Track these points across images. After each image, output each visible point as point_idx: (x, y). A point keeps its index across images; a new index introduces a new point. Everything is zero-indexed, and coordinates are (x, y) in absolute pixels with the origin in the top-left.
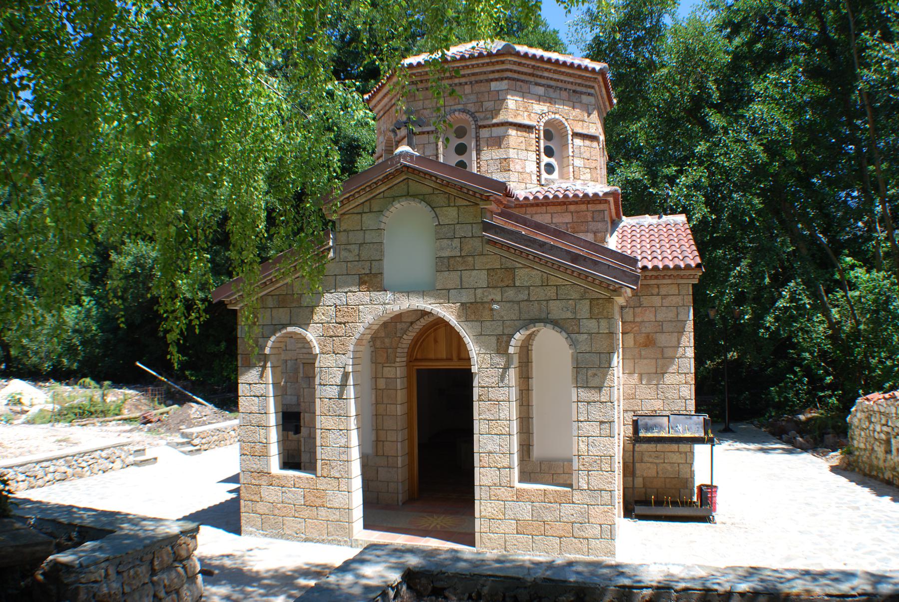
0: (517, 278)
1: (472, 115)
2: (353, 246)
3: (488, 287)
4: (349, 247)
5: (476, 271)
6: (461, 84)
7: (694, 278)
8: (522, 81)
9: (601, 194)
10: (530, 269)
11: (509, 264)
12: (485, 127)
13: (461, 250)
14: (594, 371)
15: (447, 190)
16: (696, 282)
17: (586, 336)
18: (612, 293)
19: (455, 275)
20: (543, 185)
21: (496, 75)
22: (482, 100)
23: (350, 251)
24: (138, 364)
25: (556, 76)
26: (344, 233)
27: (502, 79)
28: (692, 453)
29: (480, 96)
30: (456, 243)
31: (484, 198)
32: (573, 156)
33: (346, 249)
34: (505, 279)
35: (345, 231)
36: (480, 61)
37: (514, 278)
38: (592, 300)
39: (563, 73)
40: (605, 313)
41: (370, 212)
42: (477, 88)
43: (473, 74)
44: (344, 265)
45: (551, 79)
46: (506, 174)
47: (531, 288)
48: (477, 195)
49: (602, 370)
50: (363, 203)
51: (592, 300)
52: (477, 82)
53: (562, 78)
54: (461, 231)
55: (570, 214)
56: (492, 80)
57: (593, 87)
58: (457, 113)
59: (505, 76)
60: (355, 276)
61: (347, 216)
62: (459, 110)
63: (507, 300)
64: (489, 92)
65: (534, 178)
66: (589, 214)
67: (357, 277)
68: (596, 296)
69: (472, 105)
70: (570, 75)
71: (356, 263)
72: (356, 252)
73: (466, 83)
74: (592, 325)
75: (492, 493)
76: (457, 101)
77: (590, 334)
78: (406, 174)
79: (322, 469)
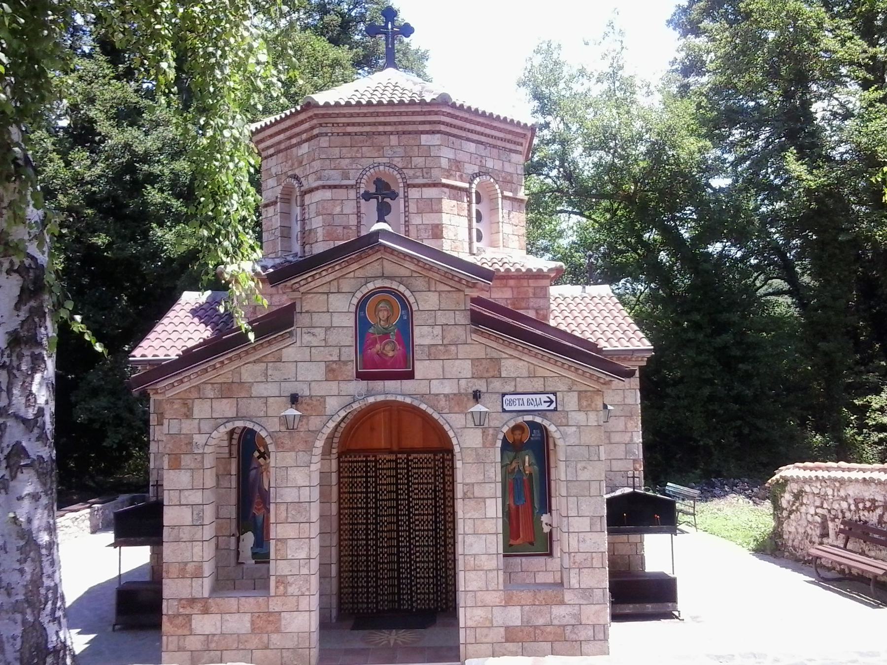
0: (503, 369)
1: (400, 171)
2: (318, 329)
4: (313, 330)
5: (460, 361)
6: (385, 133)
7: (642, 360)
8: (454, 136)
9: (545, 270)
11: (495, 355)
12: (414, 186)
13: (443, 338)
14: (583, 464)
15: (430, 274)
16: (644, 364)
17: (574, 429)
18: (602, 386)
19: (437, 364)
20: (474, 254)
21: (427, 127)
22: (411, 154)
24: (527, 458)
25: (488, 131)
26: (306, 314)
27: (434, 132)
28: (642, 542)
29: (408, 149)
30: (438, 330)
31: (470, 285)
32: (503, 222)
34: (490, 370)
35: (307, 312)
37: (500, 369)
38: (580, 392)
39: (495, 128)
40: (593, 405)
41: (338, 292)
42: (405, 139)
43: (400, 123)
45: (482, 134)
46: (438, 242)
47: (518, 379)
50: (330, 282)
51: (580, 392)
52: (404, 133)
53: (494, 133)
54: (442, 319)
55: (510, 289)
56: (422, 132)
57: (522, 145)
58: (382, 168)
59: (438, 129)
63: (494, 391)
65: (466, 246)
66: (531, 290)
68: (584, 388)
69: (399, 159)
71: (322, 349)
73: (392, 133)
74: (580, 417)
75: (478, 599)
76: (381, 152)
77: (579, 427)
78: (382, 254)
79: (277, 587)
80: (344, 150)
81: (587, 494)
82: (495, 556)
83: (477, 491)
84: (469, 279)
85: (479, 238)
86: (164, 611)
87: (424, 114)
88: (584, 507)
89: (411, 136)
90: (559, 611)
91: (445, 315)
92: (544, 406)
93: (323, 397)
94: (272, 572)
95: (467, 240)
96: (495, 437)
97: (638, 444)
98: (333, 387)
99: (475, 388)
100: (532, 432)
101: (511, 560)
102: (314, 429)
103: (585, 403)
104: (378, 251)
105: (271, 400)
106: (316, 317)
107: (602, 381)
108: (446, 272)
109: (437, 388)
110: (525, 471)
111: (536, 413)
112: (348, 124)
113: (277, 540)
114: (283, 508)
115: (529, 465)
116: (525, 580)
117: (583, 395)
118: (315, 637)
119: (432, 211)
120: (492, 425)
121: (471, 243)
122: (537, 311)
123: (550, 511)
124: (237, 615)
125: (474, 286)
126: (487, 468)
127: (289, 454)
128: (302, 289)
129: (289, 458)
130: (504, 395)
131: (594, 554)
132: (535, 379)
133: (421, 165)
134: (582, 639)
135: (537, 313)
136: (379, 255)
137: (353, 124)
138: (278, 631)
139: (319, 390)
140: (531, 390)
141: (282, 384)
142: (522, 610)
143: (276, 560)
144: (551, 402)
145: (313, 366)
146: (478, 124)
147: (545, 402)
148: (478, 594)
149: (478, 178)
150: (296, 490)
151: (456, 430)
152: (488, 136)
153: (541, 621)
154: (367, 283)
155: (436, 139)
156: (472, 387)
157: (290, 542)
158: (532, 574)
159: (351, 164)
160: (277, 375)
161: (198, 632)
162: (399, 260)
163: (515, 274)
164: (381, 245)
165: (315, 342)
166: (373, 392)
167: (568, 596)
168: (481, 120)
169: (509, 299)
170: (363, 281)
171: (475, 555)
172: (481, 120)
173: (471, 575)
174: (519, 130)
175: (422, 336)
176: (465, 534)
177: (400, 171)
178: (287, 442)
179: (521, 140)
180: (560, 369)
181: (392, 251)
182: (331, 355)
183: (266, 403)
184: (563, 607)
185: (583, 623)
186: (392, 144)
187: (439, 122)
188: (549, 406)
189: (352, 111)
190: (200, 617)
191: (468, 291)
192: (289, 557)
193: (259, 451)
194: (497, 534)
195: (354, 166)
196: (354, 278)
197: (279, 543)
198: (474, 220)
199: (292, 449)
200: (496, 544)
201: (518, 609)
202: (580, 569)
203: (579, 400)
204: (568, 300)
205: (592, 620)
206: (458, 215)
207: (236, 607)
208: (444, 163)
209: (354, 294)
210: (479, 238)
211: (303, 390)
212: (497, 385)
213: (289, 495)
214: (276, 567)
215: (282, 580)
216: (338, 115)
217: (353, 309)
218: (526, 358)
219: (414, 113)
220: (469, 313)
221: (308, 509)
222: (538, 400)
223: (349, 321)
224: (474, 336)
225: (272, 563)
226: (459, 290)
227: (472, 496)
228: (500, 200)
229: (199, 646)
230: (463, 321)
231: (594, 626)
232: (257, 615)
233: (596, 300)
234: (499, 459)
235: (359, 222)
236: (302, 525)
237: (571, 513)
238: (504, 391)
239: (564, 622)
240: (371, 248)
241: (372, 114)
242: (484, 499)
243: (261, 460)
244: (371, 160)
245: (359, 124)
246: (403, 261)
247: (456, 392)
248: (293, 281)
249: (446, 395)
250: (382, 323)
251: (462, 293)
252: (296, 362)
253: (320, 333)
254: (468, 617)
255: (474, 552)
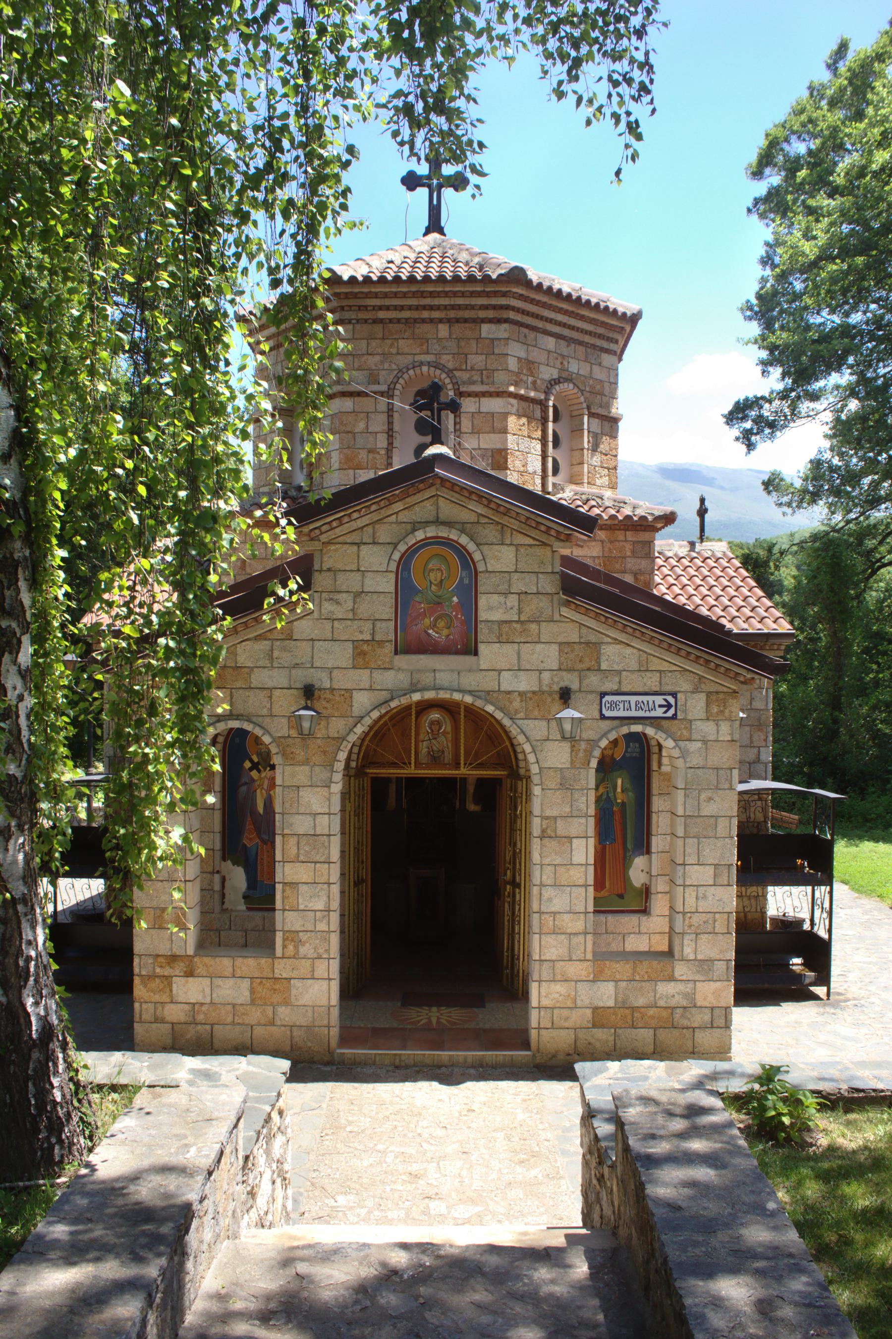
0: (603, 658)
1: (450, 372)
2: (344, 595)
3: (560, 669)
4: (337, 596)
5: (542, 646)
6: (431, 321)
8: (527, 326)
10: (622, 646)
11: (593, 638)
12: (470, 395)
13: (520, 612)
14: (709, 793)
15: (505, 520)
19: (509, 650)
21: (491, 314)
23: (338, 603)
24: (619, 781)
25: (573, 322)
27: (499, 321)
28: (764, 896)
29: (463, 344)
30: (513, 600)
31: (562, 537)
33: (331, 599)
34: (586, 659)
35: (329, 570)
36: (470, 288)
37: (598, 658)
38: (709, 694)
39: (582, 318)
41: (374, 543)
42: (458, 329)
43: (453, 307)
44: (328, 625)
47: (624, 673)
48: (553, 533)
49: (720, 792)
50: (362, 528)
52: (458, 321)
56: (484, 321)
58: (425, 369)
59: (505, 316)
60: (346, 643)
61: (333, 547)
62: (429, 364)
64: (478, 339)
66: (628, 547)
67: (350, 645)
69: (449, 357)
70: (592, 321)
71: (349, 622)
72: (350, 604)
73: (441, 321)
74: (708, 729)
75: (557, 971)
76: (425, 347)
77: (705, 742)
79: (284, 947)
80: (374, 344)
81: (711, 834)
82: (582, 916)
83: (561, 828)
84: (561, 529)
85: (556, 471)
86: (136, 970)
87: (488, 295)
88: (706, 852)
89: (467, 325)
90: (666, 989)
91: (523, 579)
92: (659, 712)
93: (349, 691)
94: (278, 926)
95: (539, 472)
96: (589, 755)
97: (766, 764)
98: (363, 677)
99: (562, 684)
100: (627, 746)
101: (602, 917)
102: (336, 735)
103: (715, 709)
104: (432, 485)
105: (277, 693)
106: (341, 577)
107: (742, 679)
108: (528, 518)
109: (508, 682)
110: (616, 799)
111: (647, 722)
112: (380, 308)
113: (285, 884)
114: (293, 841)
115: (623, 791)
116: (609, 944)
117: (714, 697)
118: (335, 1012)
119: (493, 431)
120: (584, 736)
121: (544, 477)
122: (635, 575)
123: (648, 852)
124: (231, 981)
125: (568, 538)
126: (576, 796)
127: (302, 768)
128: (324, 538)
129: (301, 774)
130: (603, 695)
131: (717, 916)
132: (647, 673)
133: (481, 365)
134: (695, 1025)
135: (636, 579)
136: (432, 492)
137: (388, 308)
138: (286, 1002)
139: (342, 681)
140: (641, 689)
141: (294, 672)
142: (616, 987)
143: (284, 910)
144: (669, 706)
145: (336, 646)
146: (560, 311)
147: (660, 706)
148: (559, 965)
149: (557, 387)
150: (309, 818)
151: (534, 743)
152: (572, 328)
153: (641, 1002)
154: (414, 530)
155: (501, 331)
156: (558, 683)
157: (303, 888)
158: (620, 937)
159: (382, 362)
160: (286, 658)
161: (181, 999)
162: (462, 498)
163: (609, 522)
164: (437, 476)
165: (339, 613)
166: (419, 686)
167: (680, 970)
168: (564, 306)
169: (598, 557)
170: (409, 527)
171: (555, 913)
172: (564, 306)
173: (549, 940)
174: (614, 322)
175: (490, 608)
176: (542, 885)
177: (450, 372)
178: (300, 754)
179: (616, 336)
180: (683, 660)
181: (453, 486)
182: (361, 632)
183: (270, 697)
184: (673, 984)
185: (699, 1004)
186: (440, 336)
187: (508, 307)
188: (665, 712)
189: (387, 290)
190: (183, 980)
191: (557, 545)
192: (302, 907)
193: (251, 761)
194: (586, 886)
195: (386, 366)
196: (397, 523)
197: (287, 888)
198: (550, 445)
199: (306, 762)
200: (585, 899)
201: (611, 986)
202: (697, 934)
203: (708, 704)
204: (673, 562)
205: (711, 1001)
206: (529, 437)
207: (231, 969)
208: (513, 364)
209: (395, 545)
210: (556, 471)
211: (323, 681)
212: (594, 681)
213: (302, 825)
214: (284, 920)
215: (292, 937)
216: (367, 295)
217: (393, 567)
218: (636, 643)
219: (473, 294)
220: (558, 577)
221: (326, 844)
222: (651, 703)
223: (387, 584)
224: (565, 611)
225: (278, 915)
226: (545, 544)
227: (553, 835)
228: (586, 418)
229: (182, 1018)
230: (550, 589)
231: (712, 1008)
232: (258, 981)
233: (711, 562)
234: (592, 784)
235: (390, 444)
236: (318, 865)
237: (689, 860)
238: (603, 689)
239: (673, 1003)
240: (422, 481)
241: (414, 294)
242: (570, 839)
243: (254, 773)
244: (410, 358)
245: (396, 308)
246: (466, 500)
247: (536, 689)
248: (312, 526)
249: (521, 694)
250: (433, 587)
251: (549, 548)
252: (312, 640)
253: (347, 601)
254: (543, 993)
255: (553, 909)
